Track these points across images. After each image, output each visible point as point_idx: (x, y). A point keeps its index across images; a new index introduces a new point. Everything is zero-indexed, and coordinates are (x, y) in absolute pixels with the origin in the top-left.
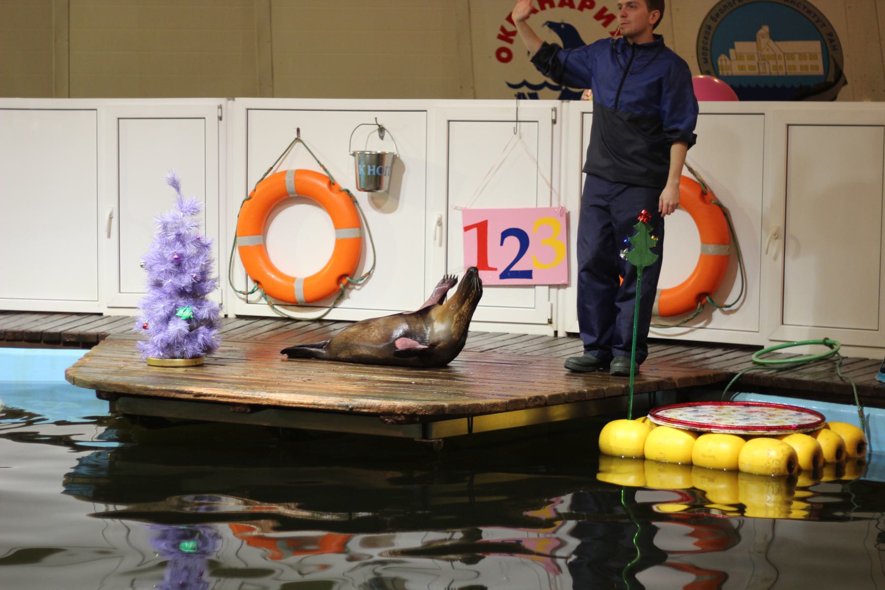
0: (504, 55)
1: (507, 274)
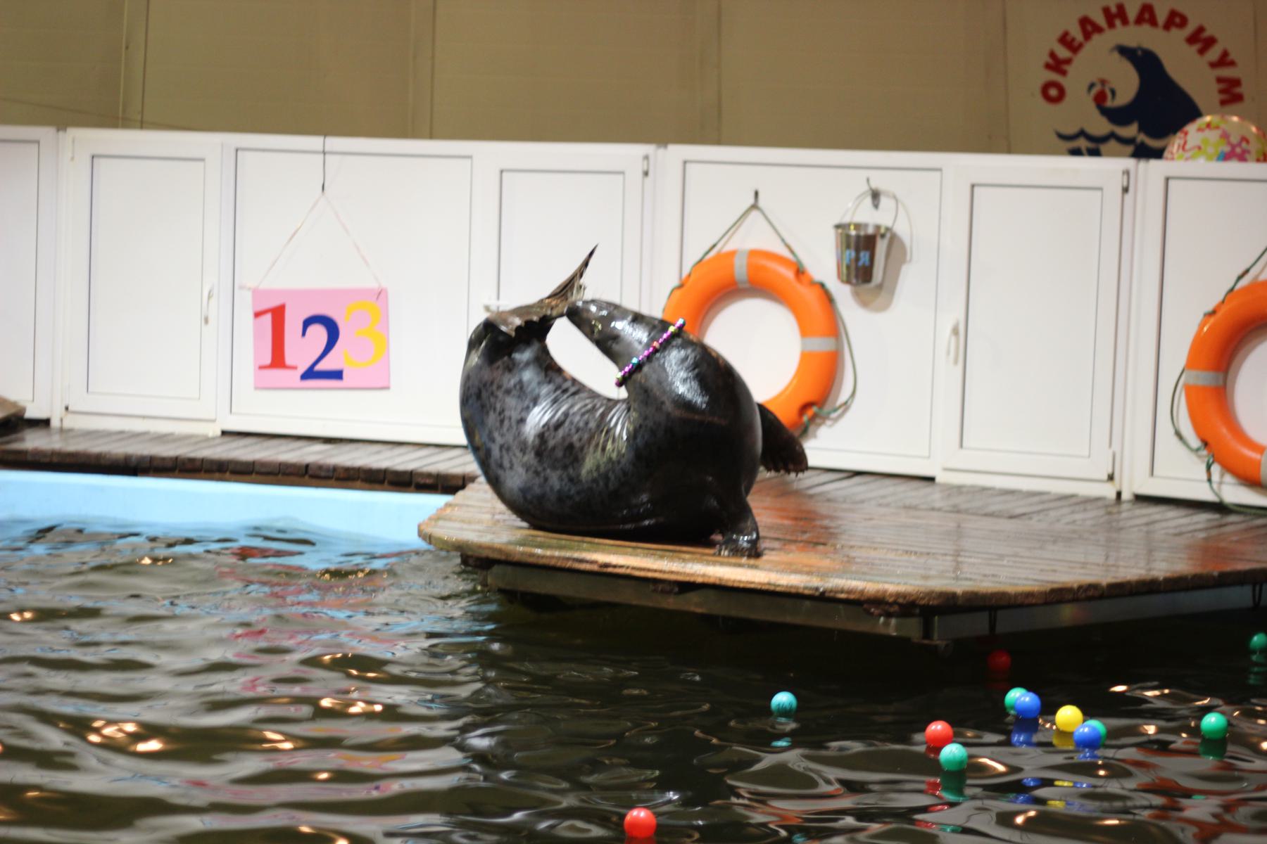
0: (1053, 92)
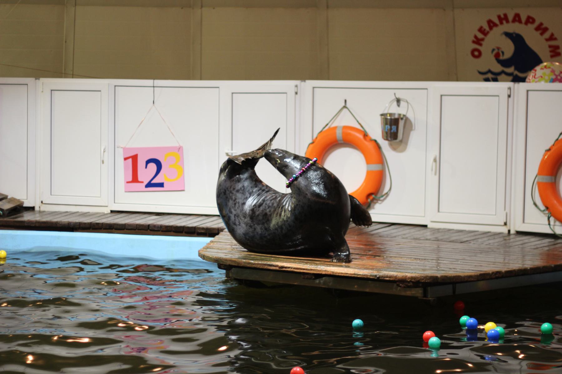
1: (150, 185)
